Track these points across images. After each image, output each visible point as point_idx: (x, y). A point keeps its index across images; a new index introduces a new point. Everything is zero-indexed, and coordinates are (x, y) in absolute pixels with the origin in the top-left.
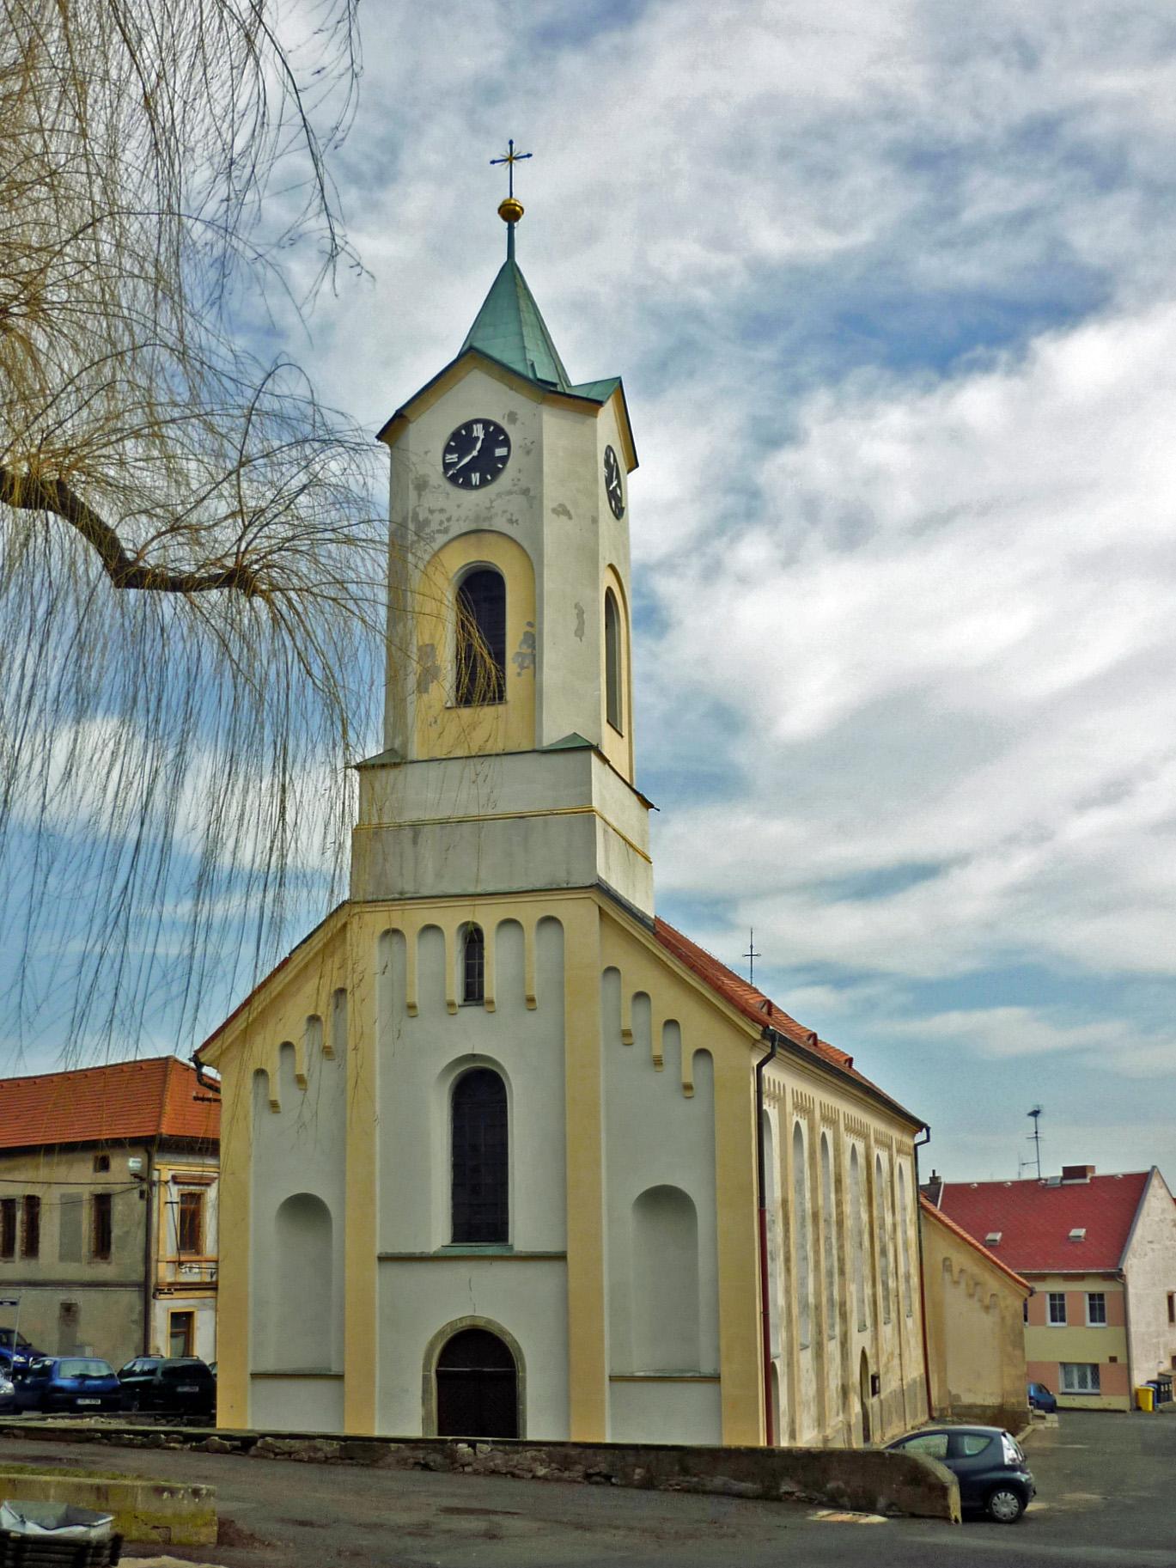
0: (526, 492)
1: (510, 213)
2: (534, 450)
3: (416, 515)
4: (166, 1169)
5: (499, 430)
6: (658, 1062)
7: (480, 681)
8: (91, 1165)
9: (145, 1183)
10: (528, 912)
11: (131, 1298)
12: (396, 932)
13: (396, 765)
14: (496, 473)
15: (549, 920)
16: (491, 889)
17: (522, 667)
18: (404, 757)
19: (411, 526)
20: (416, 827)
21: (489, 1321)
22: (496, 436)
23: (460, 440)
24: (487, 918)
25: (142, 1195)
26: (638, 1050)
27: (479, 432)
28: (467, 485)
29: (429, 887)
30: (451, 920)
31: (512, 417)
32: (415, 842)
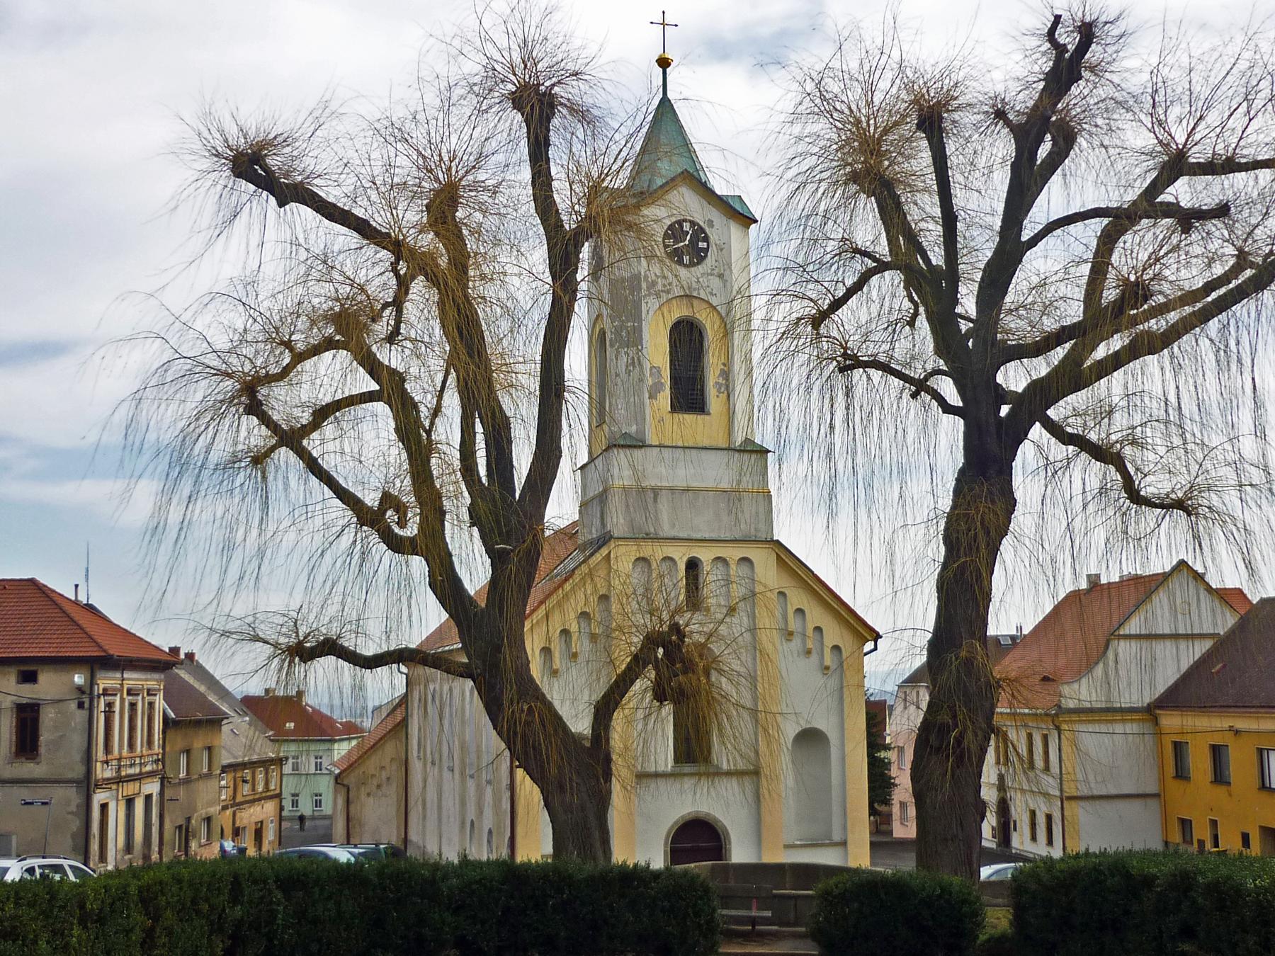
0: (721, 276)
1: (664, 63)
2: (724, 248)
3: (646, 276)
4: (106, 681)
5: (702, 230)
6: (809, 652)
7: (689, 395)
8: (13, 679)
9: (85, 697)
10: (733, 553)
11: (72, 795)
12: (644, 559)
13: (641, 447)
14: (701, 260)
15: (745, 560)
16: (707, 536)
17: (719, 391)
18: (643, 441)
19: (644, 285)
20: (656, 491)
21: (708, 814)
22: (700, 233)
23: (675, 231)
24: (705, 555)
25: (81, 705)
26: (796, 643)
27: (686, 227)
28: (680, 262)
29: (667, 531)
30: (681, 555)
31: (710, 223)
32: (655, 500)
